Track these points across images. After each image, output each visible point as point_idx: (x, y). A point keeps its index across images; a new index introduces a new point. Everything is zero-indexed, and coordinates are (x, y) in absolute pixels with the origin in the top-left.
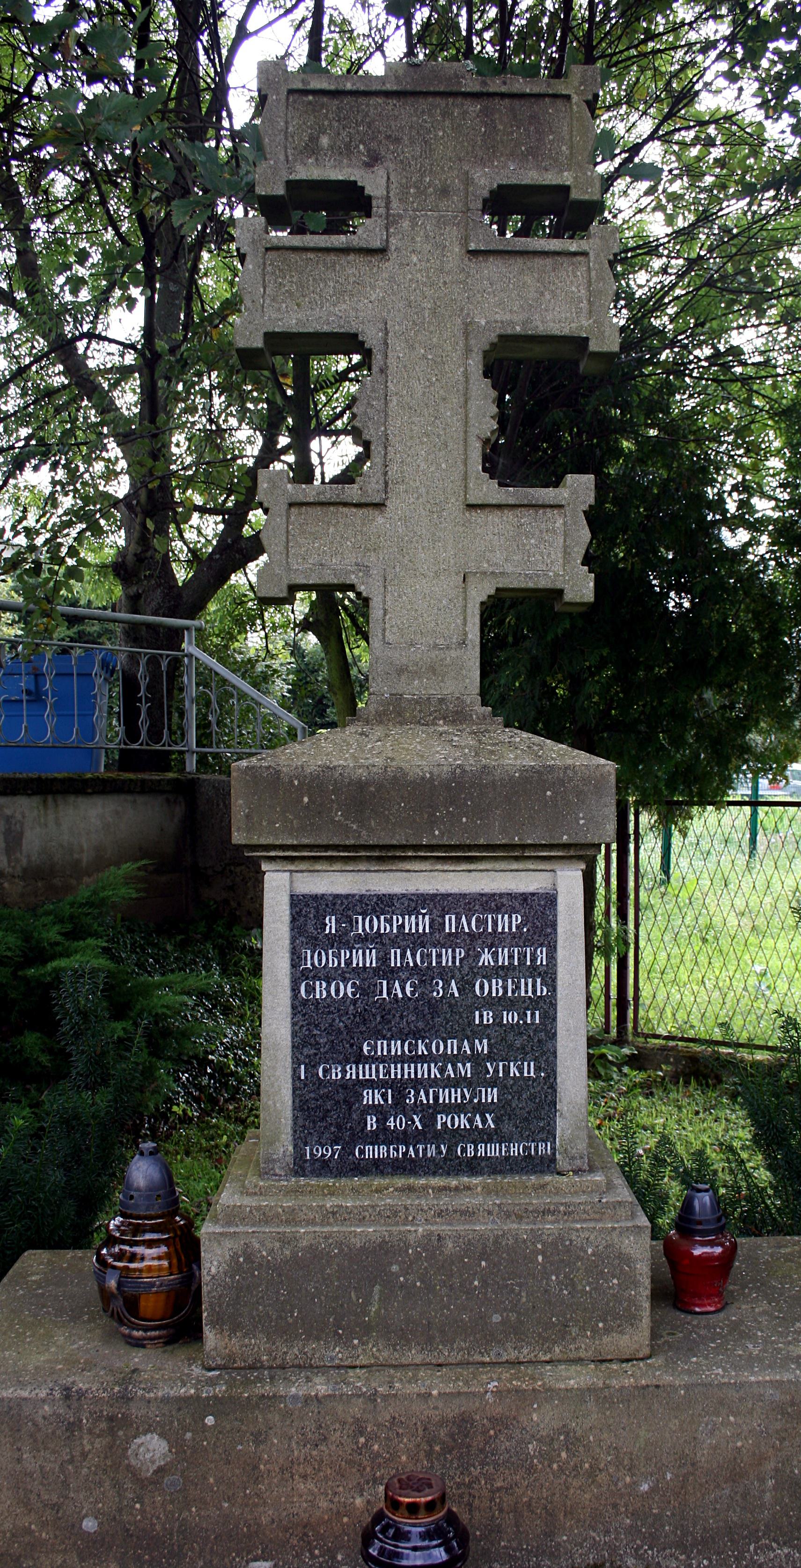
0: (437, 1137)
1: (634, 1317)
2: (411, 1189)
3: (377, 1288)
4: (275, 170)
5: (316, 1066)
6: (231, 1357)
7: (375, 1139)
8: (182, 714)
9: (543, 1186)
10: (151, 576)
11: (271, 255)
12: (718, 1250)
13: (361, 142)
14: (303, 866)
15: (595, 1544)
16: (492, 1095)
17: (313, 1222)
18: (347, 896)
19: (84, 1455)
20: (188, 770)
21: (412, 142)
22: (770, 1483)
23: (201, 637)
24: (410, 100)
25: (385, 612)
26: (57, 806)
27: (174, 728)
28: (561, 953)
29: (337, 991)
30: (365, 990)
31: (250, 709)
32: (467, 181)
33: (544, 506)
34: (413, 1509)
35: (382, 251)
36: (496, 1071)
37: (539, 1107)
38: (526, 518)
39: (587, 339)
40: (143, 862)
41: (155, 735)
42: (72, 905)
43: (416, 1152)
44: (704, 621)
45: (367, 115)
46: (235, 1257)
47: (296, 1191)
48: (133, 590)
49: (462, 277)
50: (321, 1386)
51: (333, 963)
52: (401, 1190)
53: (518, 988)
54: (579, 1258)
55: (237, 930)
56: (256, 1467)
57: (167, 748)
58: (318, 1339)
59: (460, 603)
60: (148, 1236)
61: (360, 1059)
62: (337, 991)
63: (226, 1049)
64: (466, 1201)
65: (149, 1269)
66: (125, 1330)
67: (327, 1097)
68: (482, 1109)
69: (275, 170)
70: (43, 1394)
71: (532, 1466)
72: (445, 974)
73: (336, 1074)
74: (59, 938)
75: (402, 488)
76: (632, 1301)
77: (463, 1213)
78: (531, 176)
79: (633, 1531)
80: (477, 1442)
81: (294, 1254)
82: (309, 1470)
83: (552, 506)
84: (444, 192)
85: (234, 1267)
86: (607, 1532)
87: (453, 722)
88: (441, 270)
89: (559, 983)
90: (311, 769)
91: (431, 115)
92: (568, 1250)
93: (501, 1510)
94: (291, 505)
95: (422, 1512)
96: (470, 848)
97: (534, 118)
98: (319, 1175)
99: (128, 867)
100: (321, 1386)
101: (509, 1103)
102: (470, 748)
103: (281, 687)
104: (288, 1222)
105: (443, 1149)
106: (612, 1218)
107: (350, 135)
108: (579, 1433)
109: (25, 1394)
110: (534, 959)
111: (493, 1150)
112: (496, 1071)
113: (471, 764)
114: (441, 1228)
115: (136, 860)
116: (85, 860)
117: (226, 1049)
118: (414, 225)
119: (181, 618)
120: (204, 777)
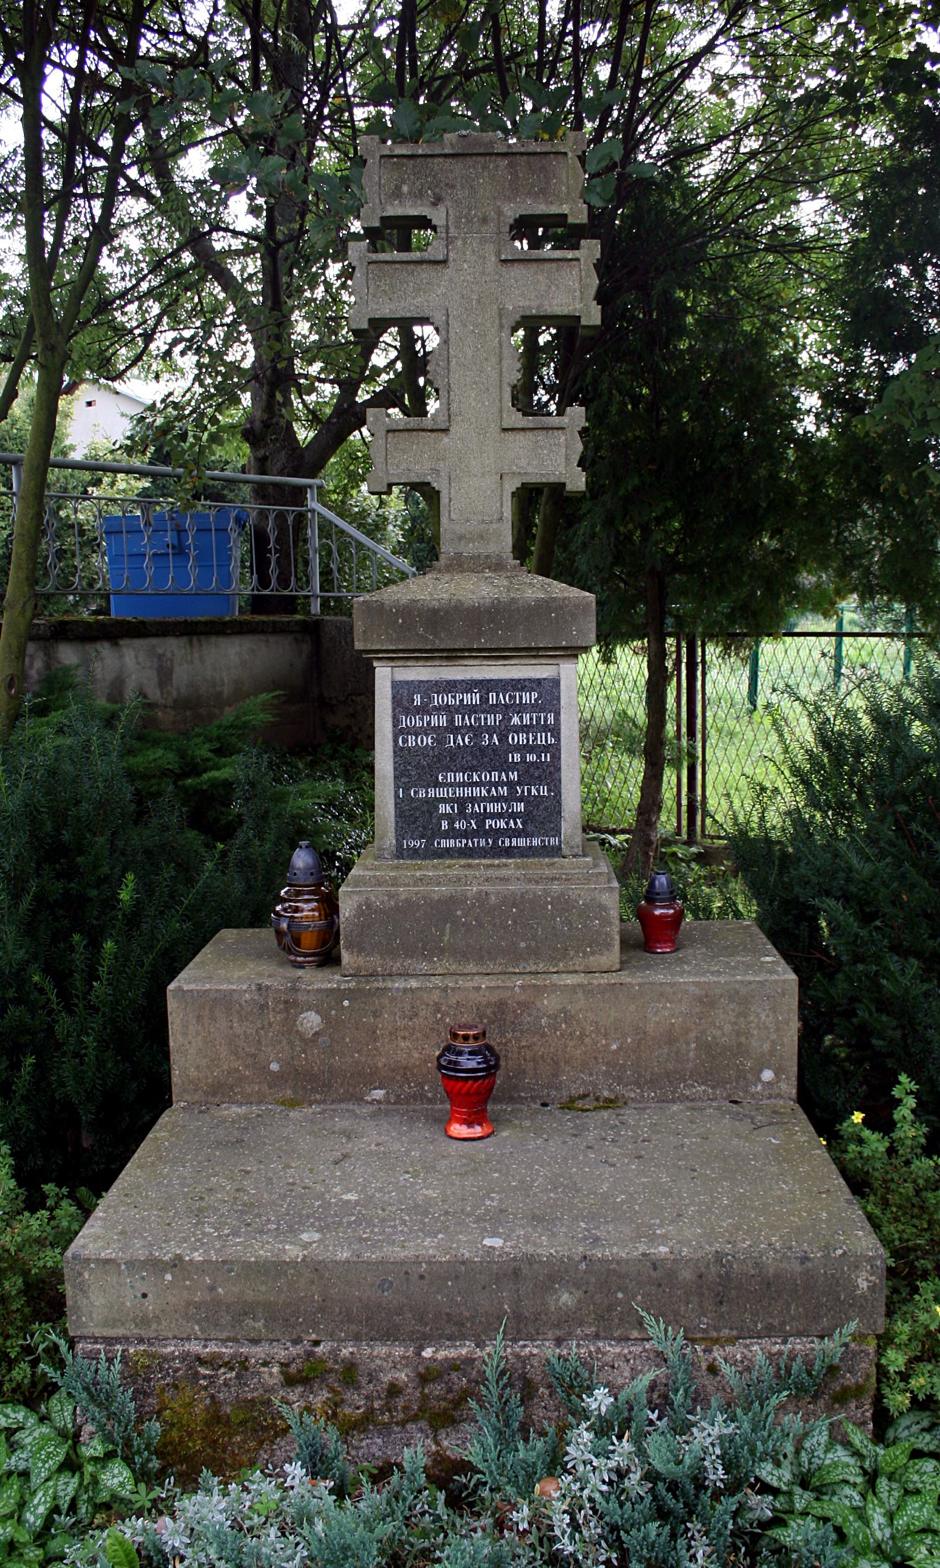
0: (486, 834)
1: (609, 945)
2: (469, 866)
3: (448, 925)
4: (373, 210)
5: (409, 789)
6: (359, 968)
7: (447, 835)
8: (306, 563)
9: (553, 864)
10: (277, 439)
11: (372, 266)
12: (672, 911)
13: (429, 188)
14: (399, 663)
15: (584, 1082)
16: (520, 807)
17: (408, 885)
18: (428, 682)
19: (270, 1024)
20: (313, 612)
21: (463, 187)
22: (693, 1045)
23: (322, 493)
24: (461, 159)
25: (450, 500)
26: (201, 645)
27: (300, 575)
28: (563, 716)
29: (422, 742)
30: (440, 741)
31: (365, 555)
32: (500, 213)
33: (552, 429)
34: (466, 1038)
35: (444, 262)
36: (523, 792)
37: (551, 814)
38: (541, 436)
39: (579, 317)
40: (277, 693)
41: (284, 582)
42: (219, 727)
43: (473, 843)
44: (753, 477)
45: (432, 170)
46: (360, 906)
47: (397, 868)
48: (261, 453)
49: (497, 277)
50: (414, 983)
51: (419, 724)
52: (464, 866)
53: (536, 739)
54: (574, 907)
55: (358, 751)
56: (374, 1032)
57: (294, 593)
58: (412, 957)
59: (498, 493)
60: (306, 897)
61: (437, 785)
62: (422, 742)
63: (352, 848)
64: (504, 872)
65: (307, 917)
66: (292, 958)
67: (416, 808)
68: (514, 816)
69: (373, 210)
70: (245, 987)
71: (544, 1032)
72: (490, 730)
73: (422, 794)
74: (210, 755)
75: (460, 418)
76: (608, 934)
77: (501, 879)
78: (541, 208)
79: (607, 1074)
80: (510, 1017)
81: (397, 904)
82: (407, 1034)
83: (557, 429)
84: (484, 220)
85: (360, 912)
86: (591, 1075)
87: (495, 570)
88: (483, 273)
89: (562, 735)
90: (403, 601)
91: (474, 168)
92: (567, 902)
93: (525, 1060)
94: (388, 431)
95: (471, 1040)
96: (504, 650)
97: (543, 169)
98: (412, 858)
99: (263, 697)
100: (414, 983)
101: (531, 812)
102: (504, 587)
103: (395, 533)
104: (392, 885)
105: (490, 841)
106: (595, 883)
107: (422, 184)
108: (573, 1012)
109: (234, 987)
110: (546, 720)
111: (521, 842)
112: (523, 792)
113: (504, 597)
114: (487, 888)
115: (270, 691)
116: (226, 692)
117: (352, 848)
118: (465, 243)
119: (303, 477)
120: (328, 618)
